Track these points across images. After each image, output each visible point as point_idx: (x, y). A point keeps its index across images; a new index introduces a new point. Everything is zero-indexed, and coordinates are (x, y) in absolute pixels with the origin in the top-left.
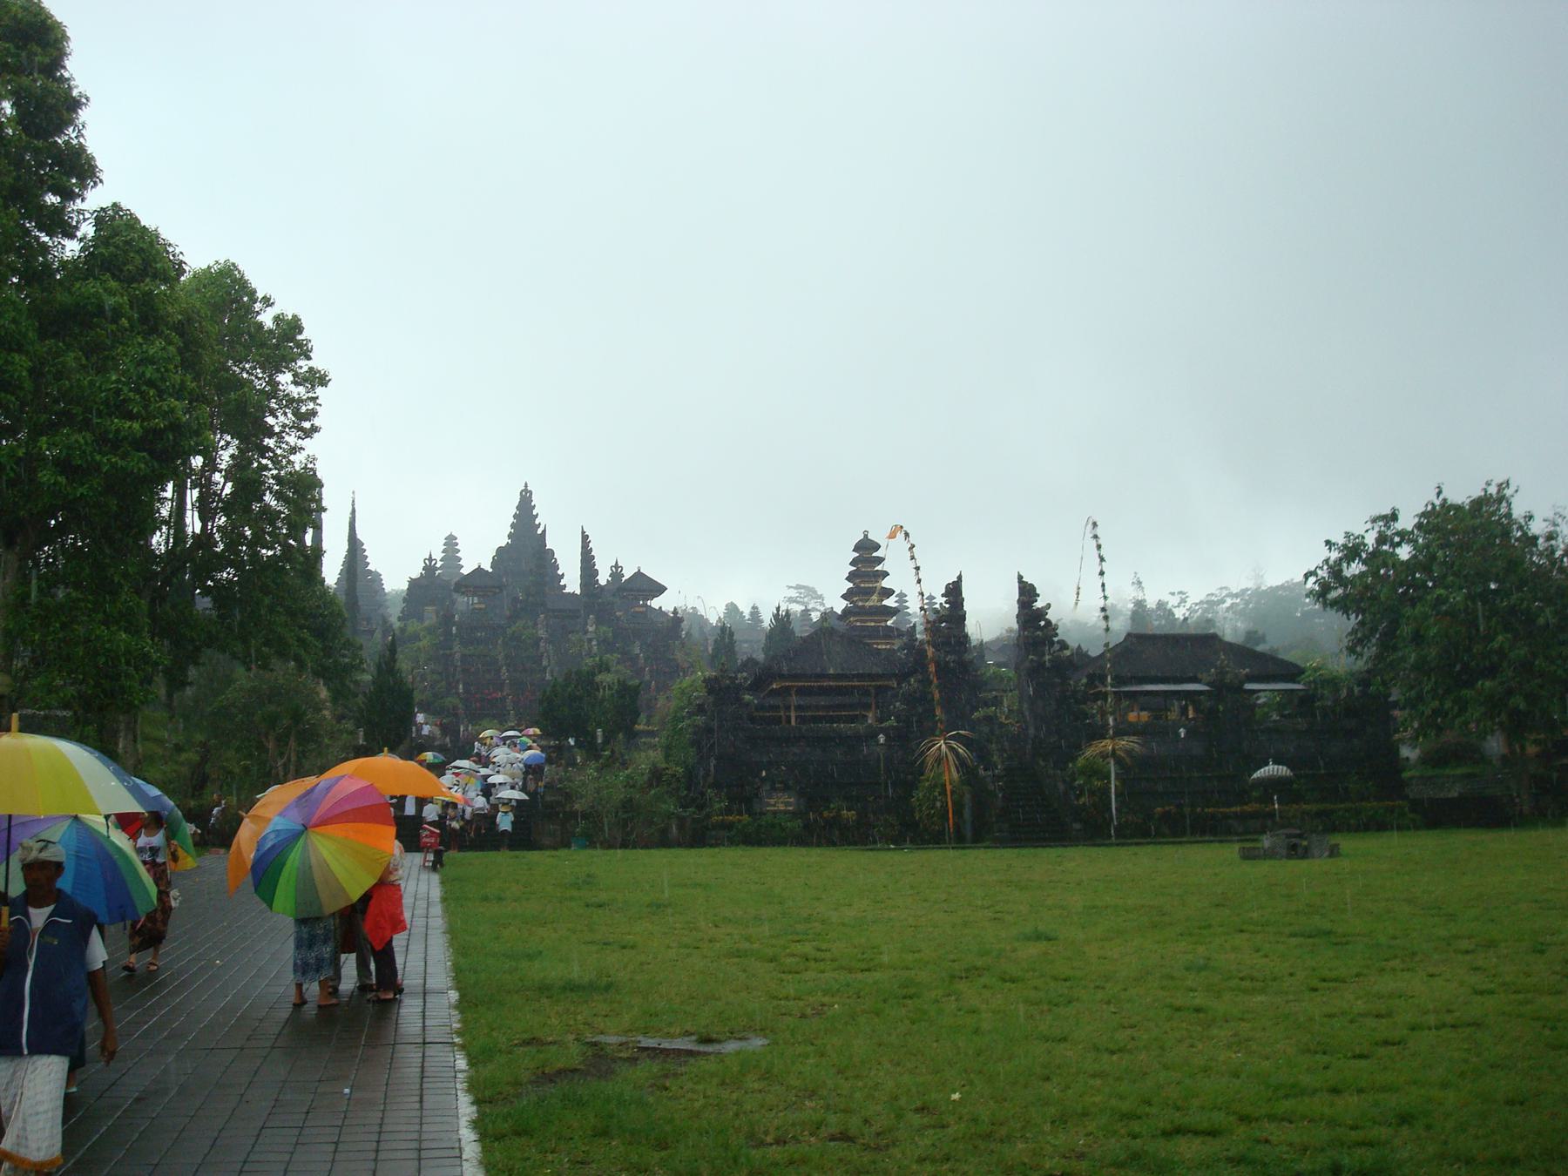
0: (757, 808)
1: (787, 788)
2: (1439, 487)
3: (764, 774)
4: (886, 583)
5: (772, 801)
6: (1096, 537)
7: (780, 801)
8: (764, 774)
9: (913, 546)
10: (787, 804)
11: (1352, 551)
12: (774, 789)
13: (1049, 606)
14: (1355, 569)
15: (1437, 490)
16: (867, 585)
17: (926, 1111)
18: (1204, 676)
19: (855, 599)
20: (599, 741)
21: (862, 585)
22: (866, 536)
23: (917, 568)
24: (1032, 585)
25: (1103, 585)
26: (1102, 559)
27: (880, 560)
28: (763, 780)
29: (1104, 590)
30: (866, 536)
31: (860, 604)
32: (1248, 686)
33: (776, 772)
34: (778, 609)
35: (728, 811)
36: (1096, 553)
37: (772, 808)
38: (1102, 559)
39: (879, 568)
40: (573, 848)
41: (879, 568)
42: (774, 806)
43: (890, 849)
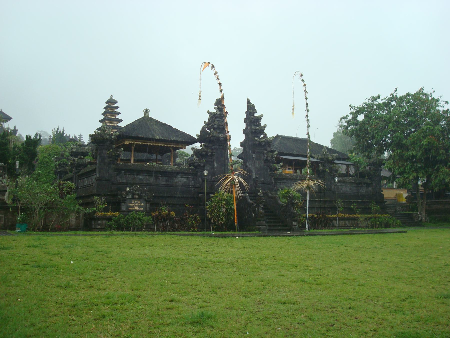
0: (124, 208)
1: (140, 198)
2: (396, 88)
3: (128, 189)
4: (118, 117)
5: (132, 205)
6: (303, 81)
7: (136, 205)
8: (128, 189)
9: (215, 74)
10: (140, 207)
11: (359, 111)
12: (133, 198)
13: (262, 115)
14: (361, 118)
15: (396, 89)
16: (111, 117)
17: (2, 309)
18: (316, 156)
19: (106, 122)
20: (17, 167)
21: (109, 117)
22: (111, 97)
23: (220, 84)
24: (253, 105)
25: (307, 104)
26: (306, 92)
27: (117, 108)
28: (128, 193)
29: (307, 107)
30: (111, 97)
31: (108, 124)
32: (336, 162)
33: (441, 152)
34: (58, 129)
35: (106, 210)
36: (303, 88)
37: (132, 209)
38: (306, 92)
39: (117, 110)
40: (17, 231)
41: (117, 110)
42: (133, 207)
43: (211, 235)
